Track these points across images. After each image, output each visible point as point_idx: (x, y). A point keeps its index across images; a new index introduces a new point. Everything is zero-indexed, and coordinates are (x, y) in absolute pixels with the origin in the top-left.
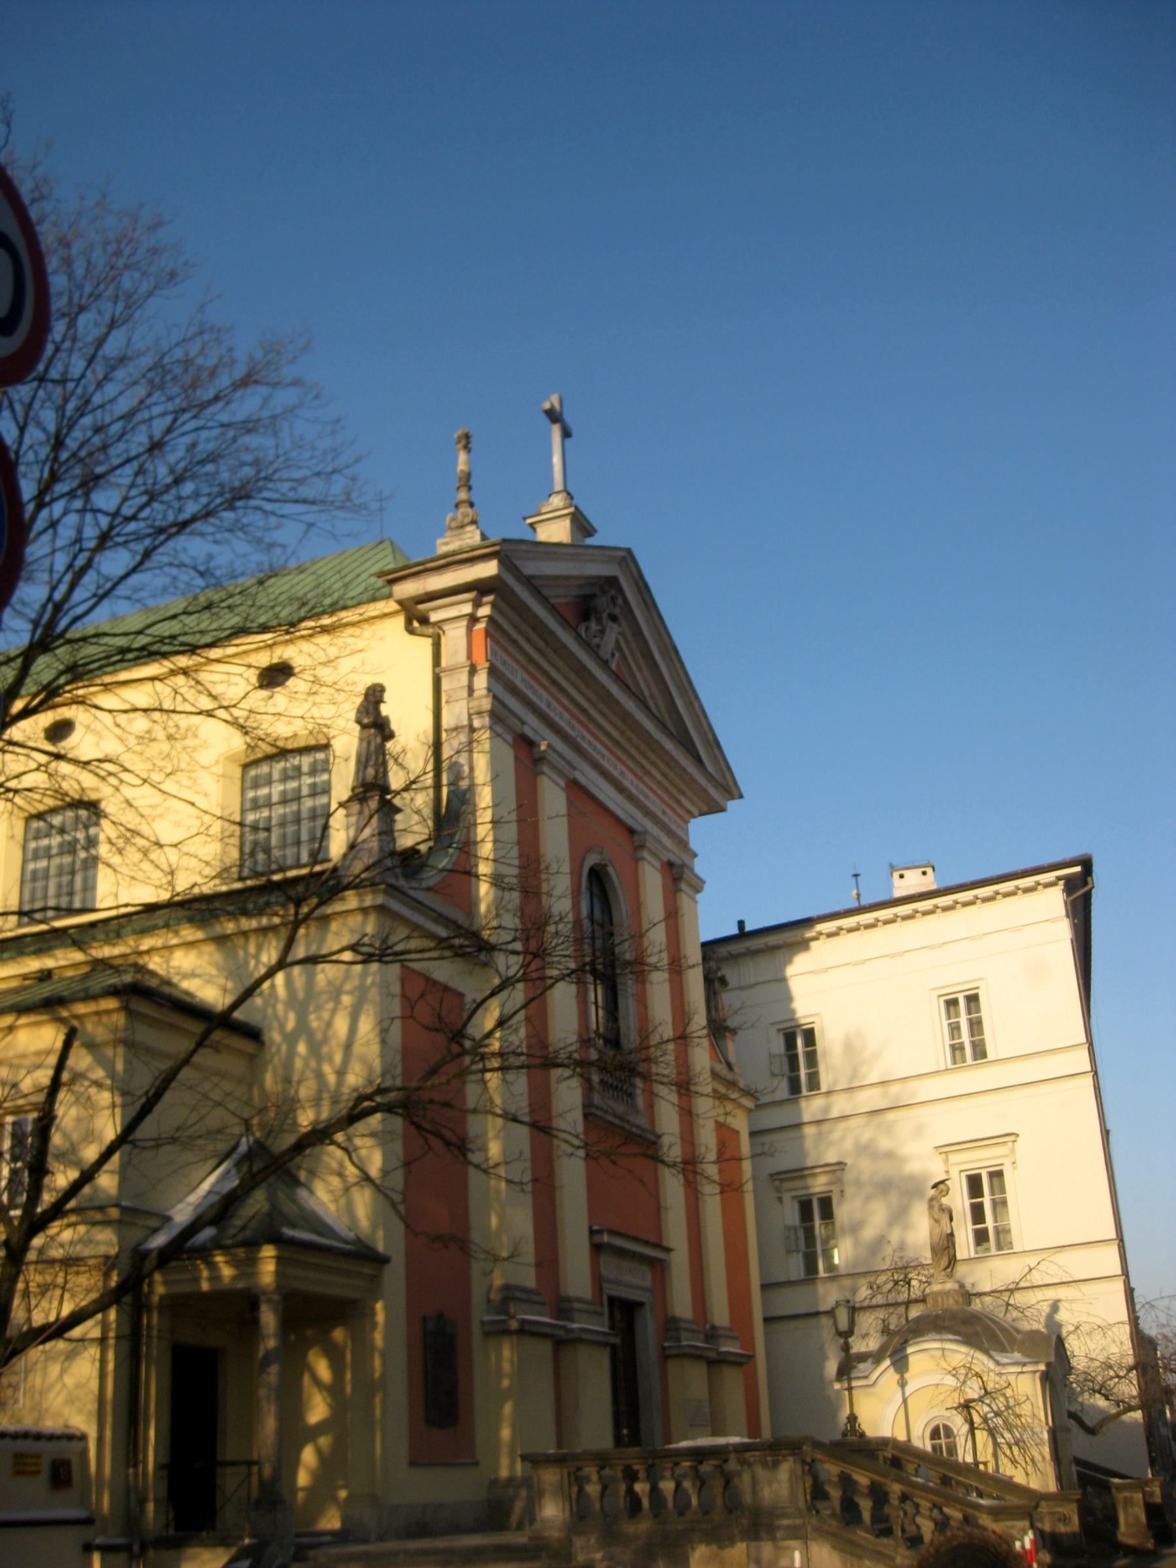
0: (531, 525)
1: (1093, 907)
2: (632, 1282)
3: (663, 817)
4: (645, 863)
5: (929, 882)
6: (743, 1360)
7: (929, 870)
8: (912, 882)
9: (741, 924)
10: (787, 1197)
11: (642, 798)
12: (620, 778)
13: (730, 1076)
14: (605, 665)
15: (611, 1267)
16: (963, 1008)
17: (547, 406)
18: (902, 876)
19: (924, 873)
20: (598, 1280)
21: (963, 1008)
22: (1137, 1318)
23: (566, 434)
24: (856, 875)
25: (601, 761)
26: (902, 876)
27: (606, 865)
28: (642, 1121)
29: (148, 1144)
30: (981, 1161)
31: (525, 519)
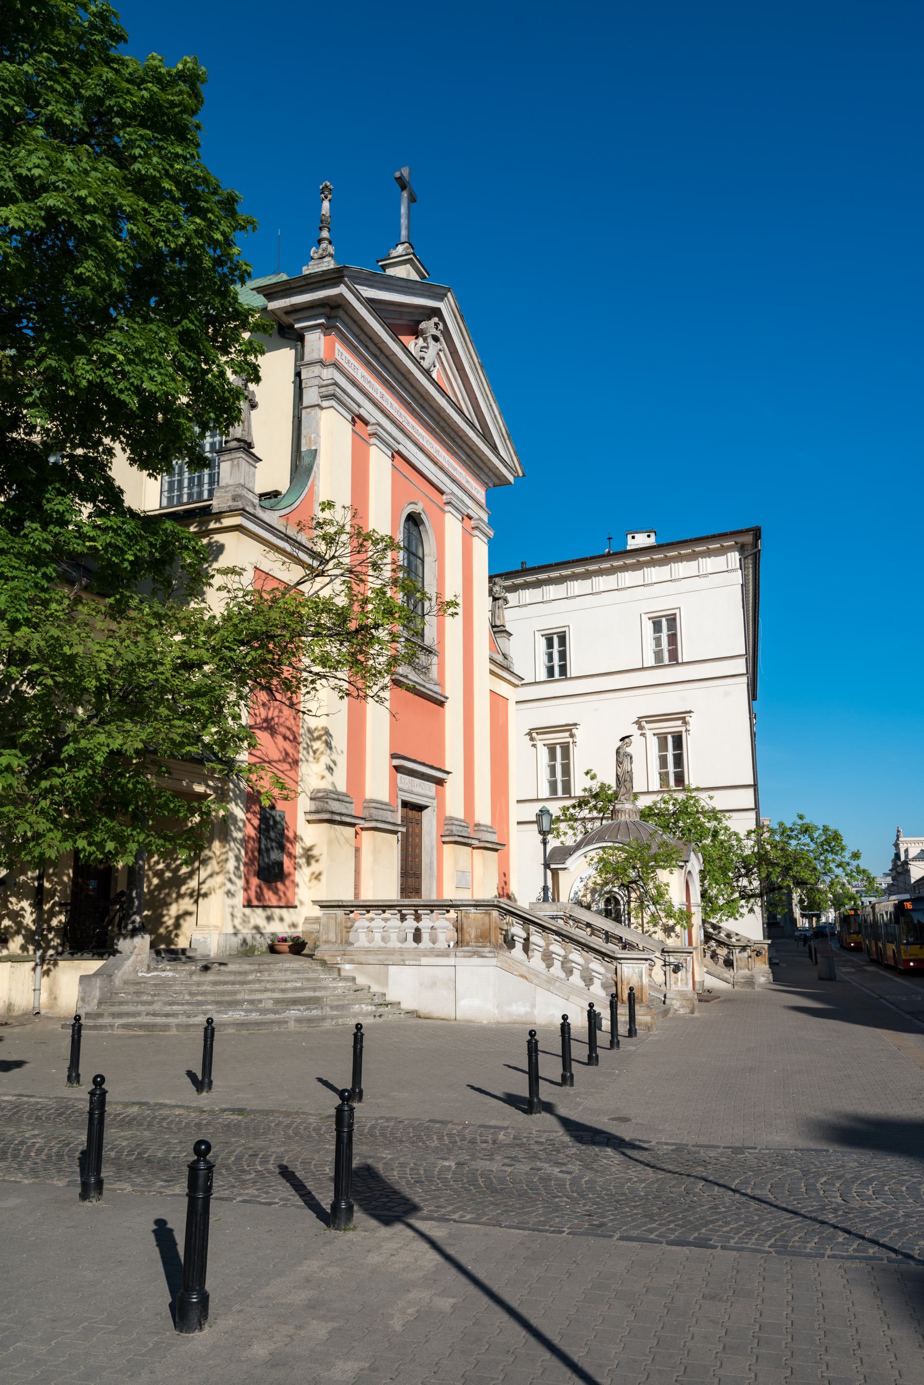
0: (382, 266)
1: (761, 564)
2: (420, 791)
3: (466, 485)
4: (474, 539)
5: (652, 541)
6: (498, 847)
7: (653, 535)
8: (641, 540)
9: (921, 948)
10: (539, 744)
11: (451, 469)
12: (380, 400)
13: (505, 663)
14: (427, 373)
15: (404, 781)
16: (667, 626)
17: (398, 174)
18: (633, 537)
19: (649, 536)
20: (394, 787)
21: (667, 626)
22: (301, 381)
23: (412, 199)
24: (610, 539)
25: (421, 441)
26: (633, 537)
27: (420, 514)
28: (437, 689)
29: (371, 958)
30: (675, 726)
31: (378, 262)
